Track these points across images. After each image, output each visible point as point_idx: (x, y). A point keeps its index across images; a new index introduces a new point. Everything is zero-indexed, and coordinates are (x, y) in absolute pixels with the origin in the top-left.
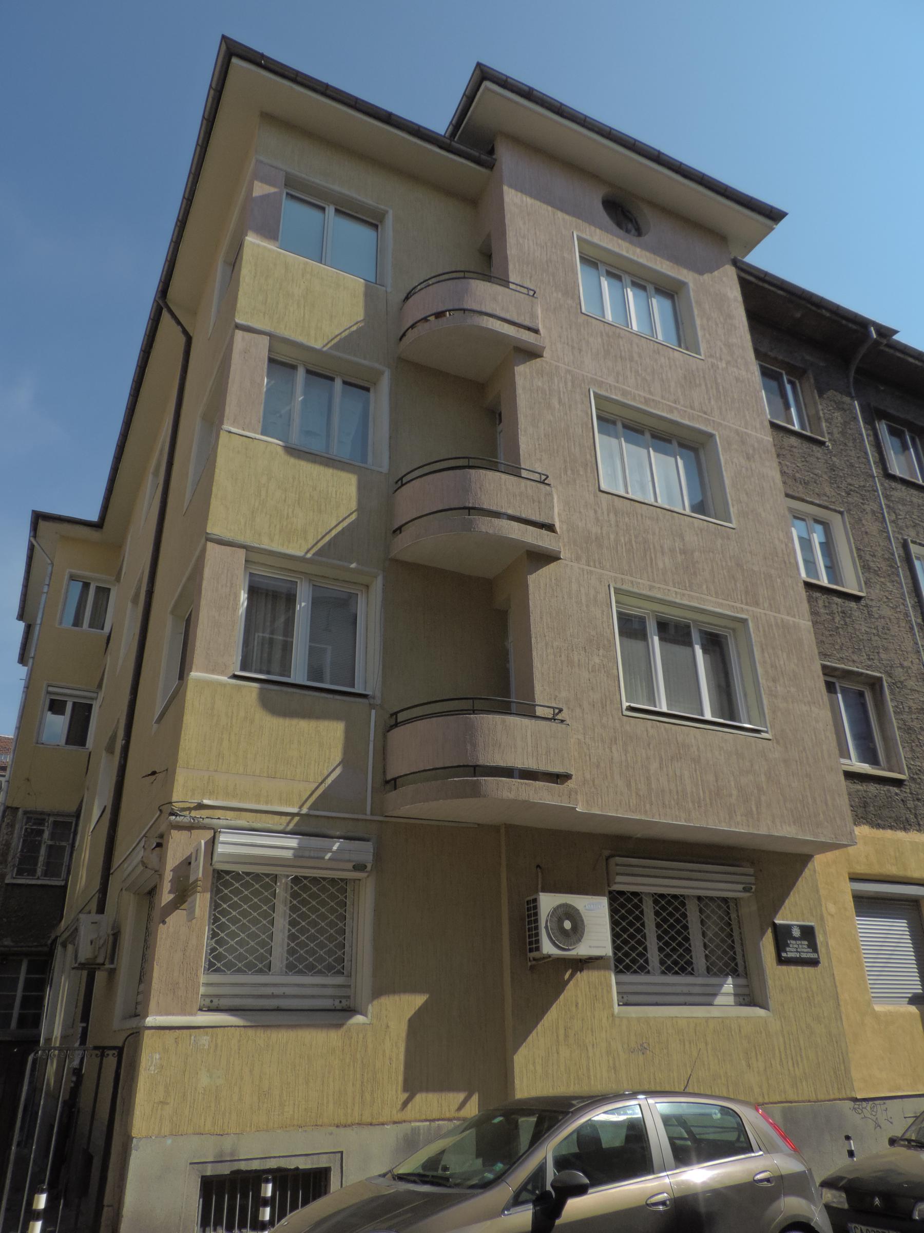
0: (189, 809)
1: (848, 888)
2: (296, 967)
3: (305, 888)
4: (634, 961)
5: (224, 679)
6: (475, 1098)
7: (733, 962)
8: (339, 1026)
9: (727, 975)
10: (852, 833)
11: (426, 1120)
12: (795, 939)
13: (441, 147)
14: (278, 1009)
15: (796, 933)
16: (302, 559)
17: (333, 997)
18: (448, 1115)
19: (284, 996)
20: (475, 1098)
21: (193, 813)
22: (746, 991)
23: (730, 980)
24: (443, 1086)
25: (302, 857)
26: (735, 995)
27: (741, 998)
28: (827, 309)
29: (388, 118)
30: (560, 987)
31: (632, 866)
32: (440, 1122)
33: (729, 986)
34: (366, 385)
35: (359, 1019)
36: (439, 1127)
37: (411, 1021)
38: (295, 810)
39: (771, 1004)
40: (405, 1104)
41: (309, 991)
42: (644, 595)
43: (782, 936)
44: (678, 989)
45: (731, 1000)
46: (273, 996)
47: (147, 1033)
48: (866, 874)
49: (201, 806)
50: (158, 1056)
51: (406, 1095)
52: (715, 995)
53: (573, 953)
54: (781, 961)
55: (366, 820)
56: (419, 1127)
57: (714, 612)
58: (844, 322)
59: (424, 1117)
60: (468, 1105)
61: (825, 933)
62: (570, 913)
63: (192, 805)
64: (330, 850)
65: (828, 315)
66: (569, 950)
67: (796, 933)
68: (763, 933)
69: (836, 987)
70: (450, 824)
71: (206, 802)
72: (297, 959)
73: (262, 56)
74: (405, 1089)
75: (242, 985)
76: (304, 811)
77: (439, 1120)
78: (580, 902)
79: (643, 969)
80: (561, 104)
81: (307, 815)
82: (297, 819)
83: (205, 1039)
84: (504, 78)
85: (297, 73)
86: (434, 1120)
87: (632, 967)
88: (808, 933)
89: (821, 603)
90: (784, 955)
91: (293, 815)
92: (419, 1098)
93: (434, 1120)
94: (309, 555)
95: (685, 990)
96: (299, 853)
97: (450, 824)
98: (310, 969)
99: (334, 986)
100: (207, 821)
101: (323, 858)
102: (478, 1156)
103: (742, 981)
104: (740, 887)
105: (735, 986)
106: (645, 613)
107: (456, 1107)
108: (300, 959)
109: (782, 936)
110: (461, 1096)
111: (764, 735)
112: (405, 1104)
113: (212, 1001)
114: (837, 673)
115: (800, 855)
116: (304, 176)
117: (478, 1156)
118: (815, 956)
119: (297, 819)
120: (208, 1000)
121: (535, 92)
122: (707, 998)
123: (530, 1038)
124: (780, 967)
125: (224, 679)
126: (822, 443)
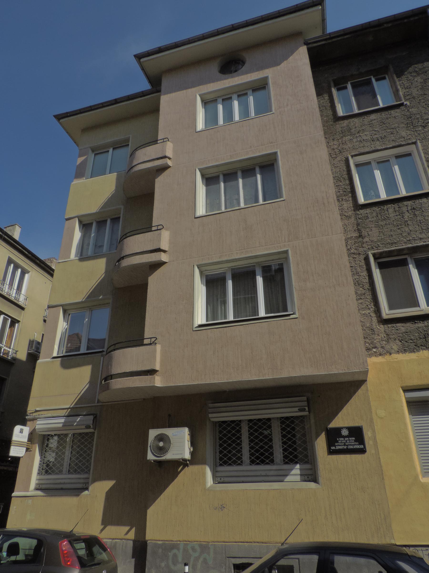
0: (33, 413)
1: (402, 397)
2: (265, 461)
3: (83, 438)
4: (230, 459)
5: (49, 360)
6: (134, 530)
7: (298, 453)
8: (78, 495)
9: (296, 463)
10: (365, 363)
11: (110, 539)
12: (344, 437)
13: (141, 97)
14: (62, 489)
15: (345, 432)
16: (82, 302)
17: (83, 483)
18: (120, 537)
19: (64, 483)
20: (134, 530)
21: (34, 414)
22: (309, 472)
23: (298, 466)
24: (119, 523)
25: (65, 426)
26: (301, 475)
27: (306, 477)
28: (387, 23)
29: (116, 102)
30: (175, 475)
31: (220, 407)
32: (117, 540)
33: (297, 470)
34: (116, 216)
35: (86, 492)
36: (116, 542)
37: (107, 493)
38: (68, 407)
39: (320, 480)
40: (102, 530)
41: (73, 481)
42: (215, 262)
43: (333, 436)
44: (258, 473)
45: (298, 478)
46: (61, 483)
47: (13, 498)
48: (419, 385)
49: (36, 411)
50: (15, 507)
51: (102, 527)
52: (286, 475)
53: (163, 458)
54: (331, 452)
55: (95, 406)
56: (107, 541)
57: (264, 254)
58: (406, 21)
59: (109, 537)
60: (130, 533)
61: (374, 431)
62: (161, 438)
63: (34, 411)
64: (75, 421)
65: (390, 25)
66: (161, 457)
67: (345, 432)
68: (318, 436)
69: (381, 467)
70: (132, 401)
71: (37, 409)
72: (269, 457)
73: (67, 113)
74: (102, 524)
75: (72, 479)
76: (71, 407)
77: (116, 539)
78: (170, 432)
79: (272, 462)
80: (175, 43)
81: (73, 408)
82: (69, 410)
83: (30, 501)
84: (147, 52)
85: (80, 110)
86: (113, 539)
87: (294, 460)
88: (357, 433)
89: (391, 211)
90: (333, 448)
91: (68, 409)
92: (109, 528)
93: (113, 539)
94: (84, 300)
95: (263, 473)
96: (65, 425)
97: (132, 401)
98: (75, 472)
99: (83, 478)
100: (38, 416)
101: (73, 425)
102: (133, 557)
103: (308, 466)
104: (296, 409)
105: (301, 469)
106: (225, 270)
107: (125, 533)
108: (257, 458)
109: (333, 436)
110: (127, 528)
111: (292, 316)
112: (102, 530)
113: (308, 477)
114: (405, 252)
115: (354, 382)
116: (96, 144)
117: (133, 557)
118: (362, 447)
119: (69, 410)
120: (38, 486)
121: (162, 47)
122: (280, 477)
123: (157, 501)
124: (330, 456)
125: (49, 360)
126: (402, 104)
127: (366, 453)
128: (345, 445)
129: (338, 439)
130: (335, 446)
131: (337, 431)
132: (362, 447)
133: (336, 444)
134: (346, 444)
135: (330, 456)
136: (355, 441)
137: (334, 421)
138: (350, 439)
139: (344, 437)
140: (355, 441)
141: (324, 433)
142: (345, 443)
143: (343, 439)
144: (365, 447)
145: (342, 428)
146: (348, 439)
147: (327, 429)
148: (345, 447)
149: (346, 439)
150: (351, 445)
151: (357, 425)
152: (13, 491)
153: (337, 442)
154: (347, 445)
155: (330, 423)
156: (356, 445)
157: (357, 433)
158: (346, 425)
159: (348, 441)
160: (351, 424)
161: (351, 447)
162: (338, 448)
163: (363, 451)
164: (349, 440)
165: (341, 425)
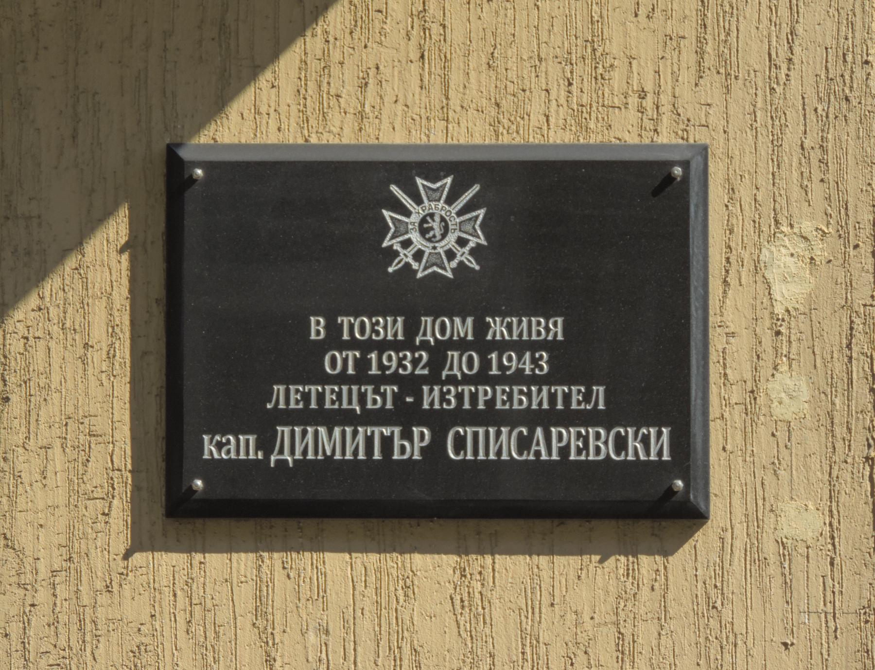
15: (433, 235)
67: (433, 235)
118: (651, 444)
127: (704, 539)
128: (406, 415)
129: (317, 327)
130: (264, 425)
131: (331, 204)
132: (651, 444)
133: (285, 396)
134: (430, 398)
135: (169, 562)
136: (568, 363)
137: (288, 63)
138: (497, 328)
139: (417, 298)
140: (568, 363)
141: (117, 228)
142: (410, 385)
143: (391, 327)
144: (688, 454)
145: (409, 169)
146: (462, 328)
147: (175, 166)
148: (412, 446)
149: (431, 330)
150: (491, 417)
151: (622, 131)
152: (445, 554)
153: (306, 365)
154: (440, 422)
155: (219, 104)
156: (568, 418)
157: (607, 249)
158: (471, 131)
159: (457, 363)
160: (548, 125)
161: (504, 445)
162: (296, 445)
163: (655, 508)
164: (482, 344)
165: (396, 124)
